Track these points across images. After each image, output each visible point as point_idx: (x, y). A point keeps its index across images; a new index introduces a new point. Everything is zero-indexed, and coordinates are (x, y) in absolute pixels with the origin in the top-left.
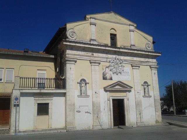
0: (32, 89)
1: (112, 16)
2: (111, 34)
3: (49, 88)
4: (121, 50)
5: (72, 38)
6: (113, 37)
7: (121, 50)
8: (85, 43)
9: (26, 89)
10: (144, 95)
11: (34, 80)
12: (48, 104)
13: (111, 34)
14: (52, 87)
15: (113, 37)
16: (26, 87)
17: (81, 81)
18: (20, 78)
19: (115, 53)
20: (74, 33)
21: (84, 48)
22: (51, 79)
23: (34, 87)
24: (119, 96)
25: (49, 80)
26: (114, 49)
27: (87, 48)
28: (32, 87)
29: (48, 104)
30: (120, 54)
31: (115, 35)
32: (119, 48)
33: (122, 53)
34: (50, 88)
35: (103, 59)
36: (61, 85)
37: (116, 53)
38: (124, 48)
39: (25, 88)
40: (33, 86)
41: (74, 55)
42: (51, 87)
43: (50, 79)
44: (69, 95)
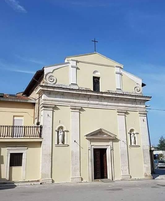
0: (18, 138)
1: (96, 57)
2: (94, 78)
3: (22, 137)
4: (104, 95)
5: (51, 83)
6: (96, 81)
7: (104, 95)
8: (64, 88)
9: (26, 138)
10: (131, 144)
11: (7, 128)
12: (21, 154)
13: (94, 78)
14: (27, 135)
15: (96, 81)
16: (34, 136)
17: (59, 129)
18: (1, 127)
19: (98, 97)
20: (136, 87)
21: (63, 93)
22: (26, 127)
23: (7, 136)
24: (100, 145)
25: (23, 128)
26: (96, 94)
27: (66, 93)
28: (5, 136)
29: (21, 154)
30: (104, 99)
31: (99, 78)
32: (102, 93)
33: (105, 98)
34: (24, 136)
35: (65, 103)
36: (38, 132)
37: (99, 97)
38: (109, 93)
39: (31, 137)
40: (6, 135)
41: (52, 101)
42: (25, 135)
43: (24, 127)
44: (45, 145)
